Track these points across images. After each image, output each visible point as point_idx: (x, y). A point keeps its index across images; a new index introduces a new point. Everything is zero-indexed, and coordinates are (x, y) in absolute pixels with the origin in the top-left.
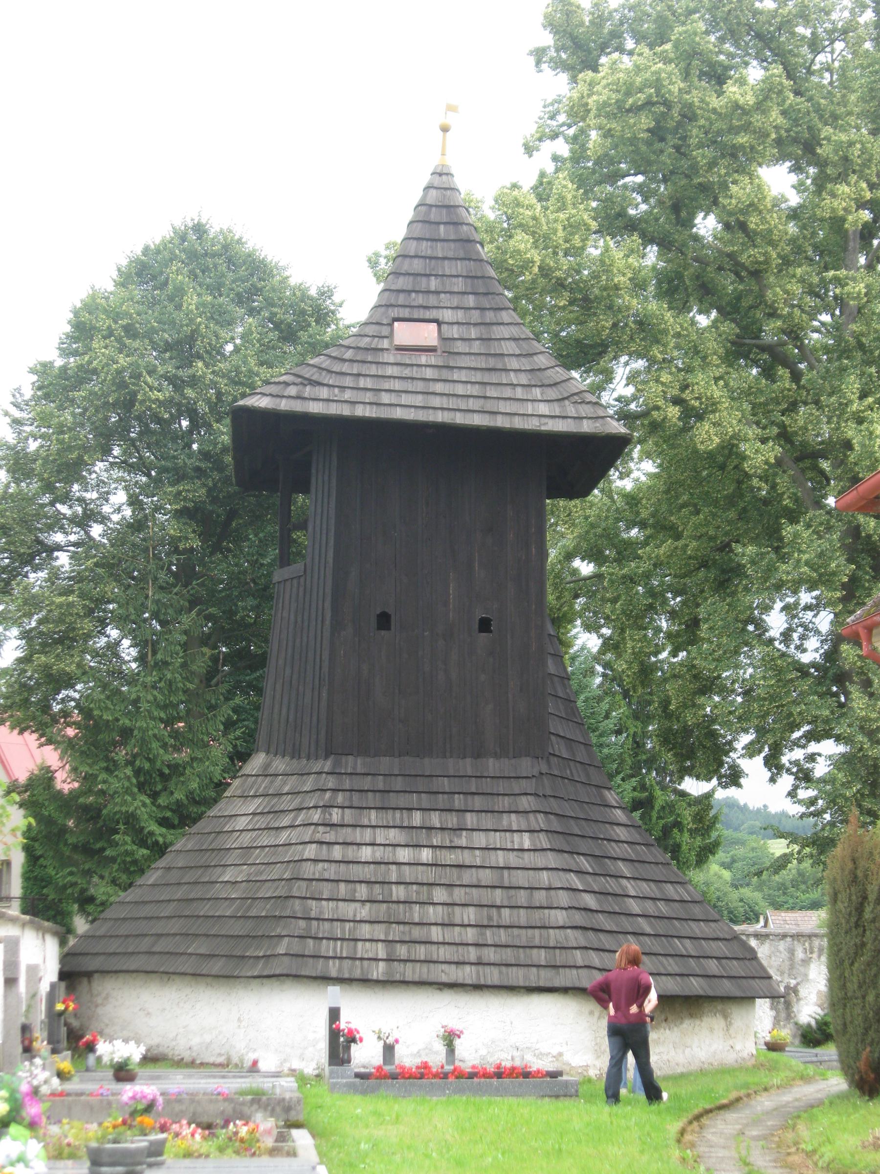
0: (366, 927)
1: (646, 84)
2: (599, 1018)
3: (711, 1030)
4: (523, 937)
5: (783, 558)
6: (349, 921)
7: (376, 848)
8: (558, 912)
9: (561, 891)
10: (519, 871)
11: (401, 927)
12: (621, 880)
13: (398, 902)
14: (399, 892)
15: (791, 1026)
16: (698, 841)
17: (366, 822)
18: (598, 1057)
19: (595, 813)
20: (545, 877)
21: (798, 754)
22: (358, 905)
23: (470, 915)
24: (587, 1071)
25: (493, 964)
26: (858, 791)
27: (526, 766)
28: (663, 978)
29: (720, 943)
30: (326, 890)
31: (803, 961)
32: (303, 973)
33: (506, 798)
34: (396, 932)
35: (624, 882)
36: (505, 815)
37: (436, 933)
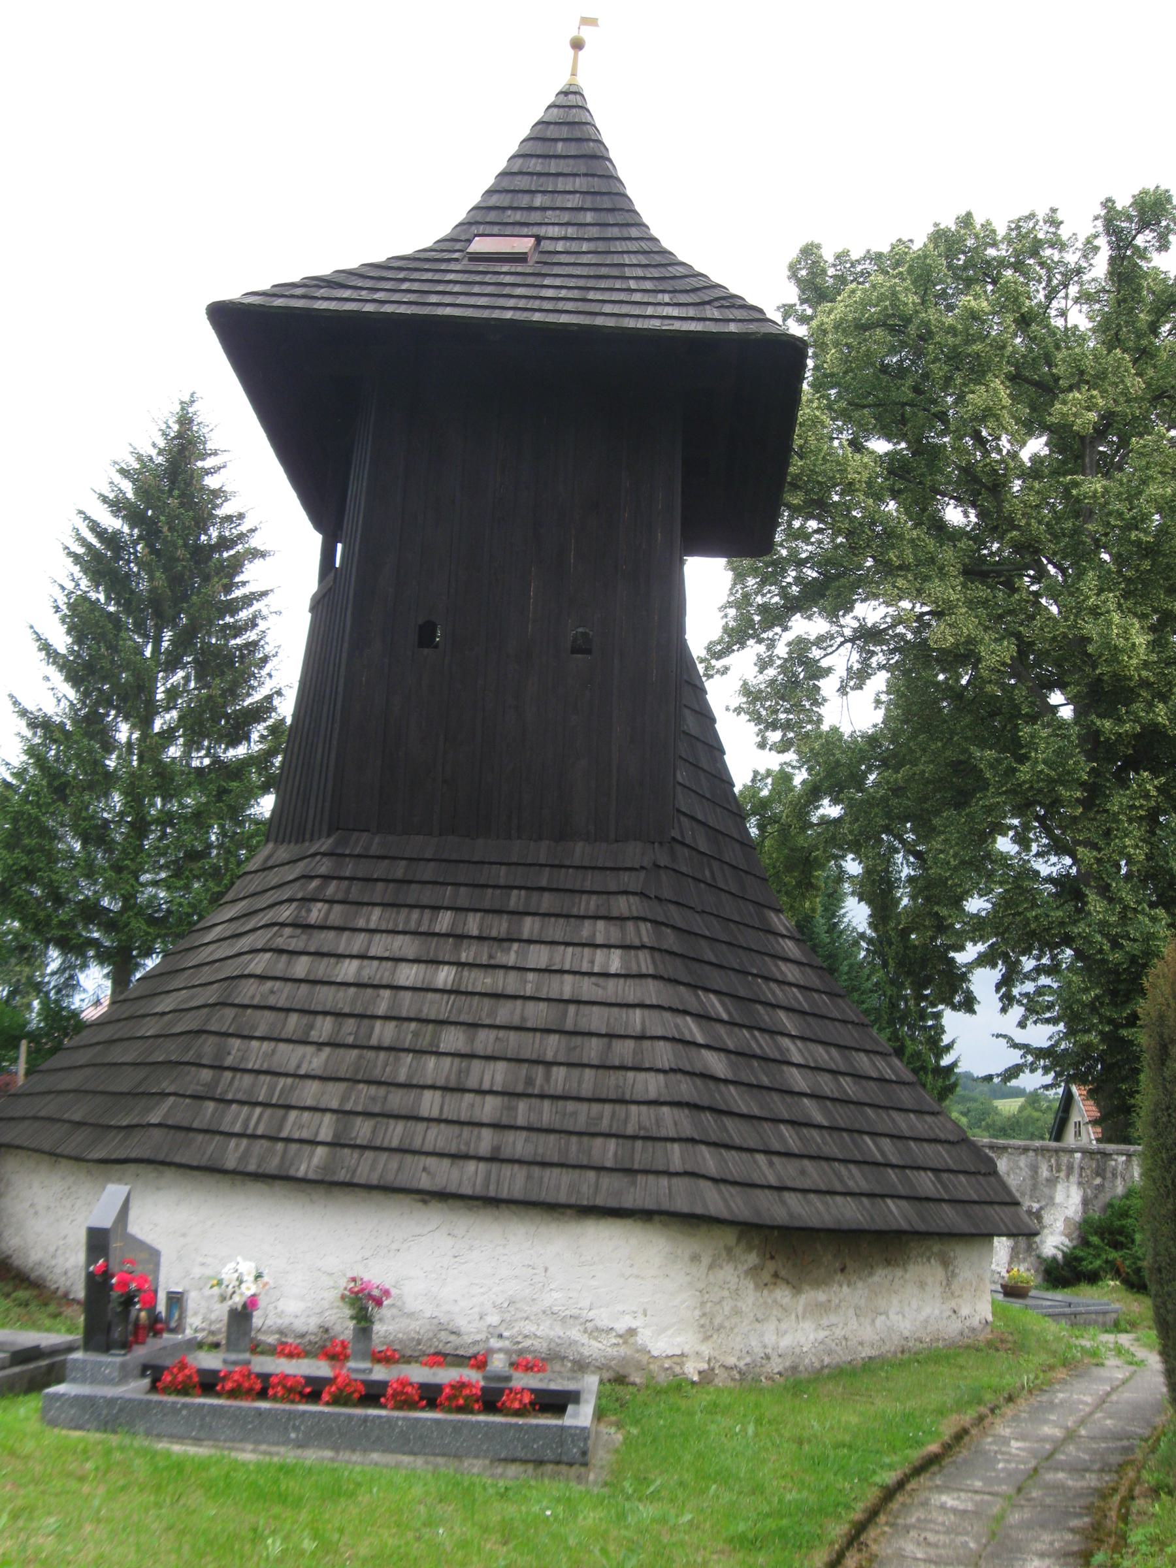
0: (313, 1087)
1: (881, 299)
2: (711, 1267)
3: (922, 1285)
4: (582, 1115)
5: (1022, 759)
6: (287, 1075)
7: (366, 962)
8: (651, 1077)
9: (662, 1043)
10: (595, 1009)
11: (373, 1090)
12: (779, 1038)
13: (379, 1048)
14: (384, 1032)
15: (1033, 1259)
16: (940, 1083)
17: (361, 923)
18: (707, 1338)
19: (748, 938)
20: (637, 1020)
21: (1029, 987)
22: (310, 1049)
23: (497, 1074)
24: (681, 1364)
25: (520, 1162)
26: (1097, 997)
27: (633, 853)
28: (839, 1199)
29: (939, 1147)
30: (264, 1022)
31: (1048, 1180)
32: (177, 1159)
33: (594, 897)
34: (362, 1097)
35: (786, 1042)
36: (587, 923)
37: (430, 1103)
